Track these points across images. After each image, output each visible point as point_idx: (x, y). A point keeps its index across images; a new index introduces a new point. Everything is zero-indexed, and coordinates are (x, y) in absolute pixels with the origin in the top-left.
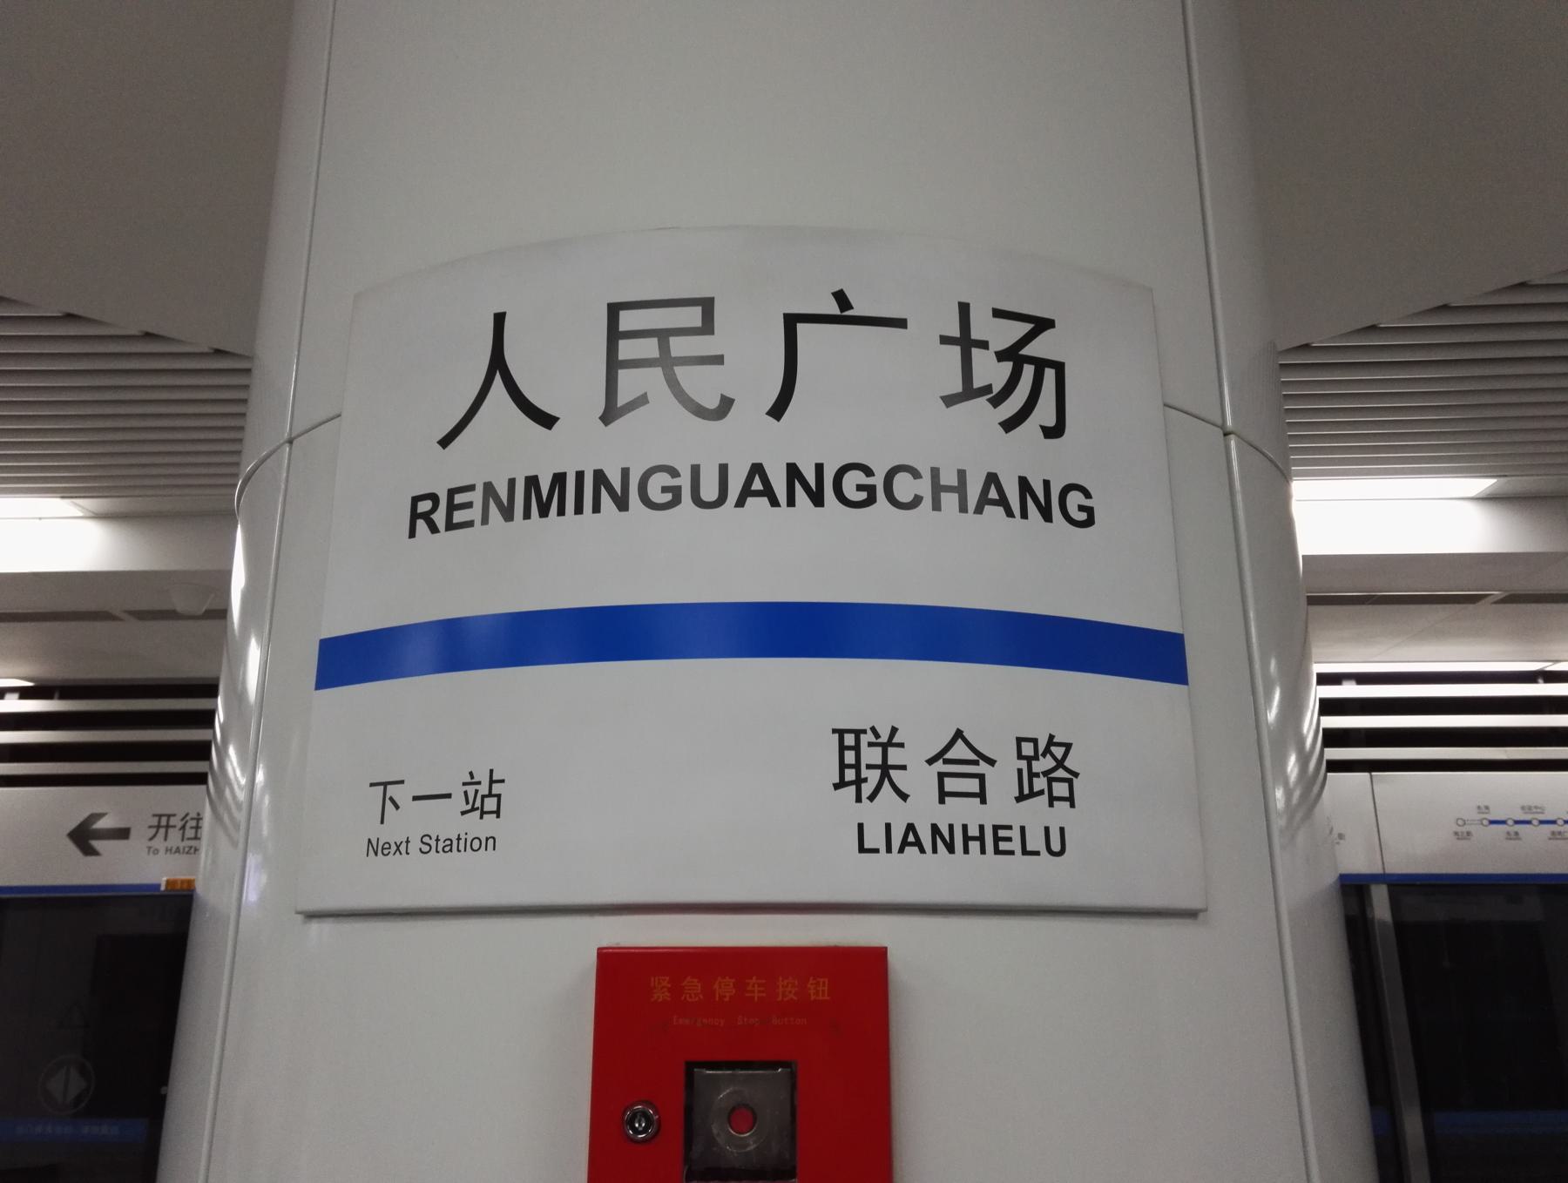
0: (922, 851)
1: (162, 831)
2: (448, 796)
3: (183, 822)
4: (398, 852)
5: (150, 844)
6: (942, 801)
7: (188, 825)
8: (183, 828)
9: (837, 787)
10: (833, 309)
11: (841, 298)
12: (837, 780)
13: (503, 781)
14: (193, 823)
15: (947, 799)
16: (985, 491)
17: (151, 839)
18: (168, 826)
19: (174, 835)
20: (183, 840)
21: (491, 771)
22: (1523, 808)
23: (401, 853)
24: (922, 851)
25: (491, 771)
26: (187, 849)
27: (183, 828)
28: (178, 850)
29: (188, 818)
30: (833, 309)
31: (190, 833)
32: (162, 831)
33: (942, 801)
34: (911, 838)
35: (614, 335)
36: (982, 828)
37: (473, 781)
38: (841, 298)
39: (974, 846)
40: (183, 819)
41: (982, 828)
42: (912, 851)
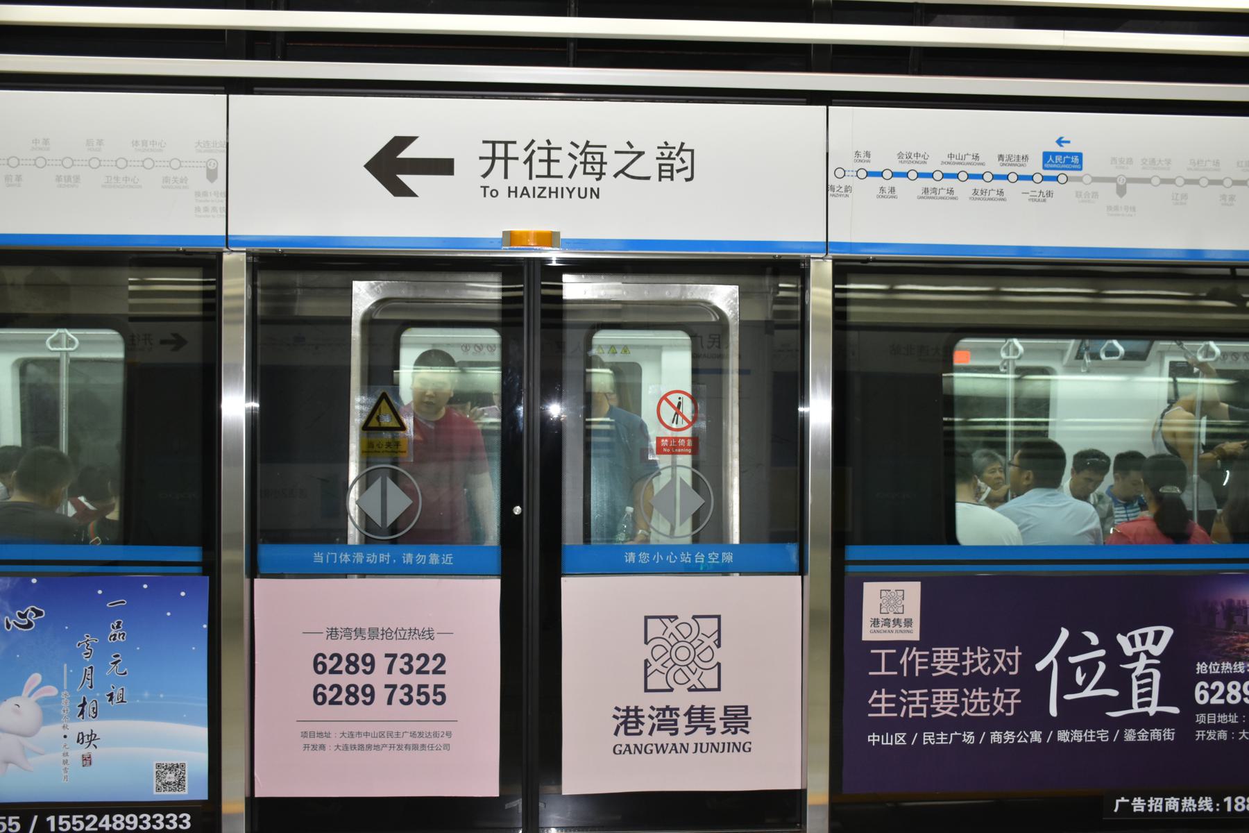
0: (529, 197)
1: (499, 164)
2: (648, 178)
3: (530, 151)
4: (571, 190)
5: (485, 182)
6: (660, 180)
7: (535, 158)
8: (529, 160)
9: (672, 179)
10: (664, 145)
11: (666, 143)
12: (670, 179)
13: (558, 161)
14: (543, 154)
15: (662, 179)
16: (523, 191)
17: (485, 176)
18: (506, 158)
19: (518, 170)
20: (531, 178)
21: (515, 142)
22: (900, 155)
23: (567, 188)
24: (529, 197)
25: (515, 142)
26: (538, 191)
27: (529, 160)
28: (525, 192)
29: (534, 147)
30: (664, 145)
31: (540, 168)
32: (499, 164)
33: (660, 180)
34: (525, 192)
35: (661, 171)
36: (557, 188)
37: (591, 165)
38: (666, 143)
39: (553, 195)
40: (526, 149)
41: (557, 188)
42: (525, 197)
